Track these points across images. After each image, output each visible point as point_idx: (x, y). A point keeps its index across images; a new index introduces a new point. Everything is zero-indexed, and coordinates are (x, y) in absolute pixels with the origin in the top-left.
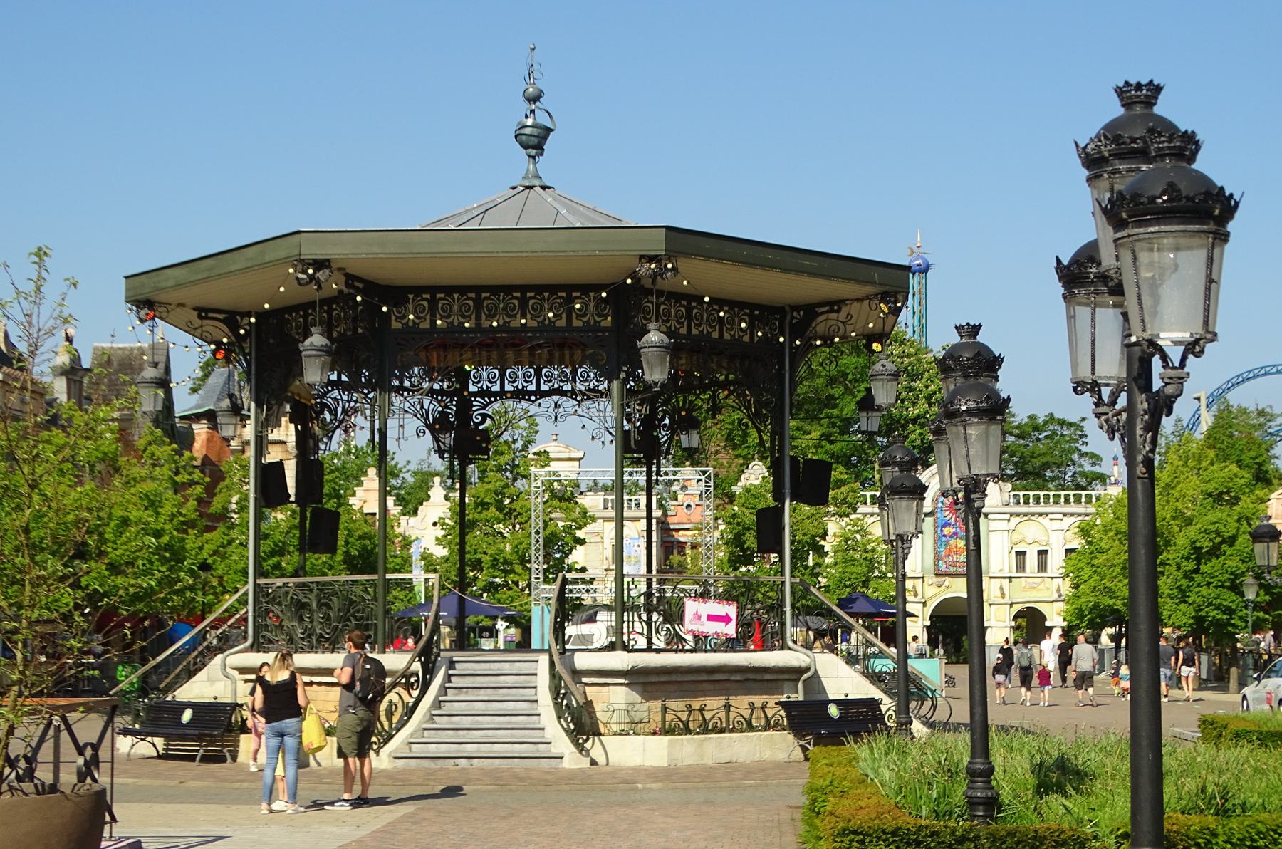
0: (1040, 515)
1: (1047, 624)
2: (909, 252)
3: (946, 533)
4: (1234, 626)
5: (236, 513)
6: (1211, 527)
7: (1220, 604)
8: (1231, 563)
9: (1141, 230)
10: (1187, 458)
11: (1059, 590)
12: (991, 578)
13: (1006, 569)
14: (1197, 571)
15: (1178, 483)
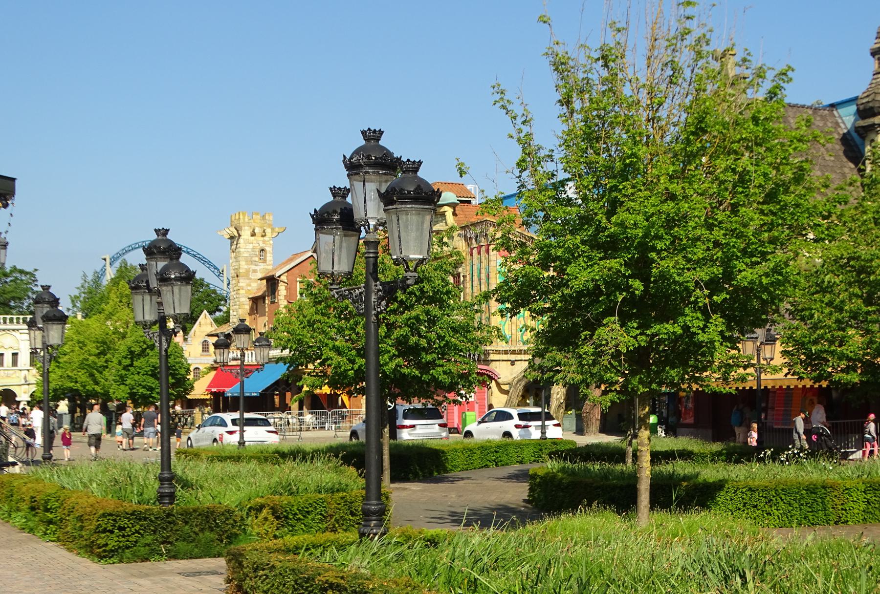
0: (14, 330)
1: (17, 399)
4: (154, 398)
6: (141, 339)
8: (152, 360)
9: (403, 206)
10: (122, 297)
11: (25, 378)
14: (131, 365)
15: (118, 312)
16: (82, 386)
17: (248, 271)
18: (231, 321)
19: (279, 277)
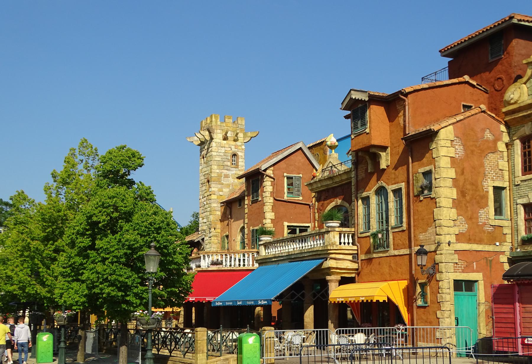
4: (128, 303)
5: (11, 302)
7: (116, 280)
14: (92, 247)
16: (20, 288)
17: (219, 176)
18: (200, 229)
19: (265, 170)
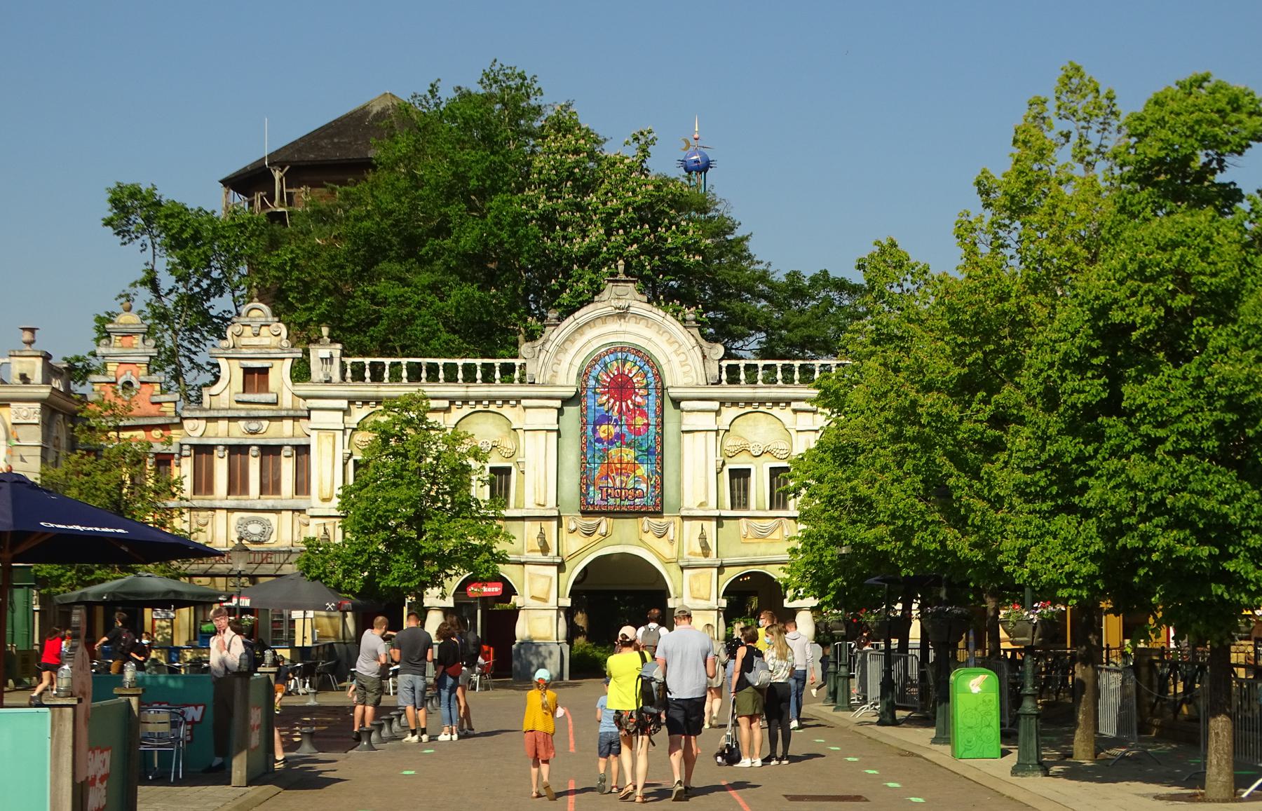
0: (776, 402)
2: (684, 145)
3: (603, 435)
4: (1234, 581)
7: (1190, 507)
12: (683, 518)
13: (713, 503)
